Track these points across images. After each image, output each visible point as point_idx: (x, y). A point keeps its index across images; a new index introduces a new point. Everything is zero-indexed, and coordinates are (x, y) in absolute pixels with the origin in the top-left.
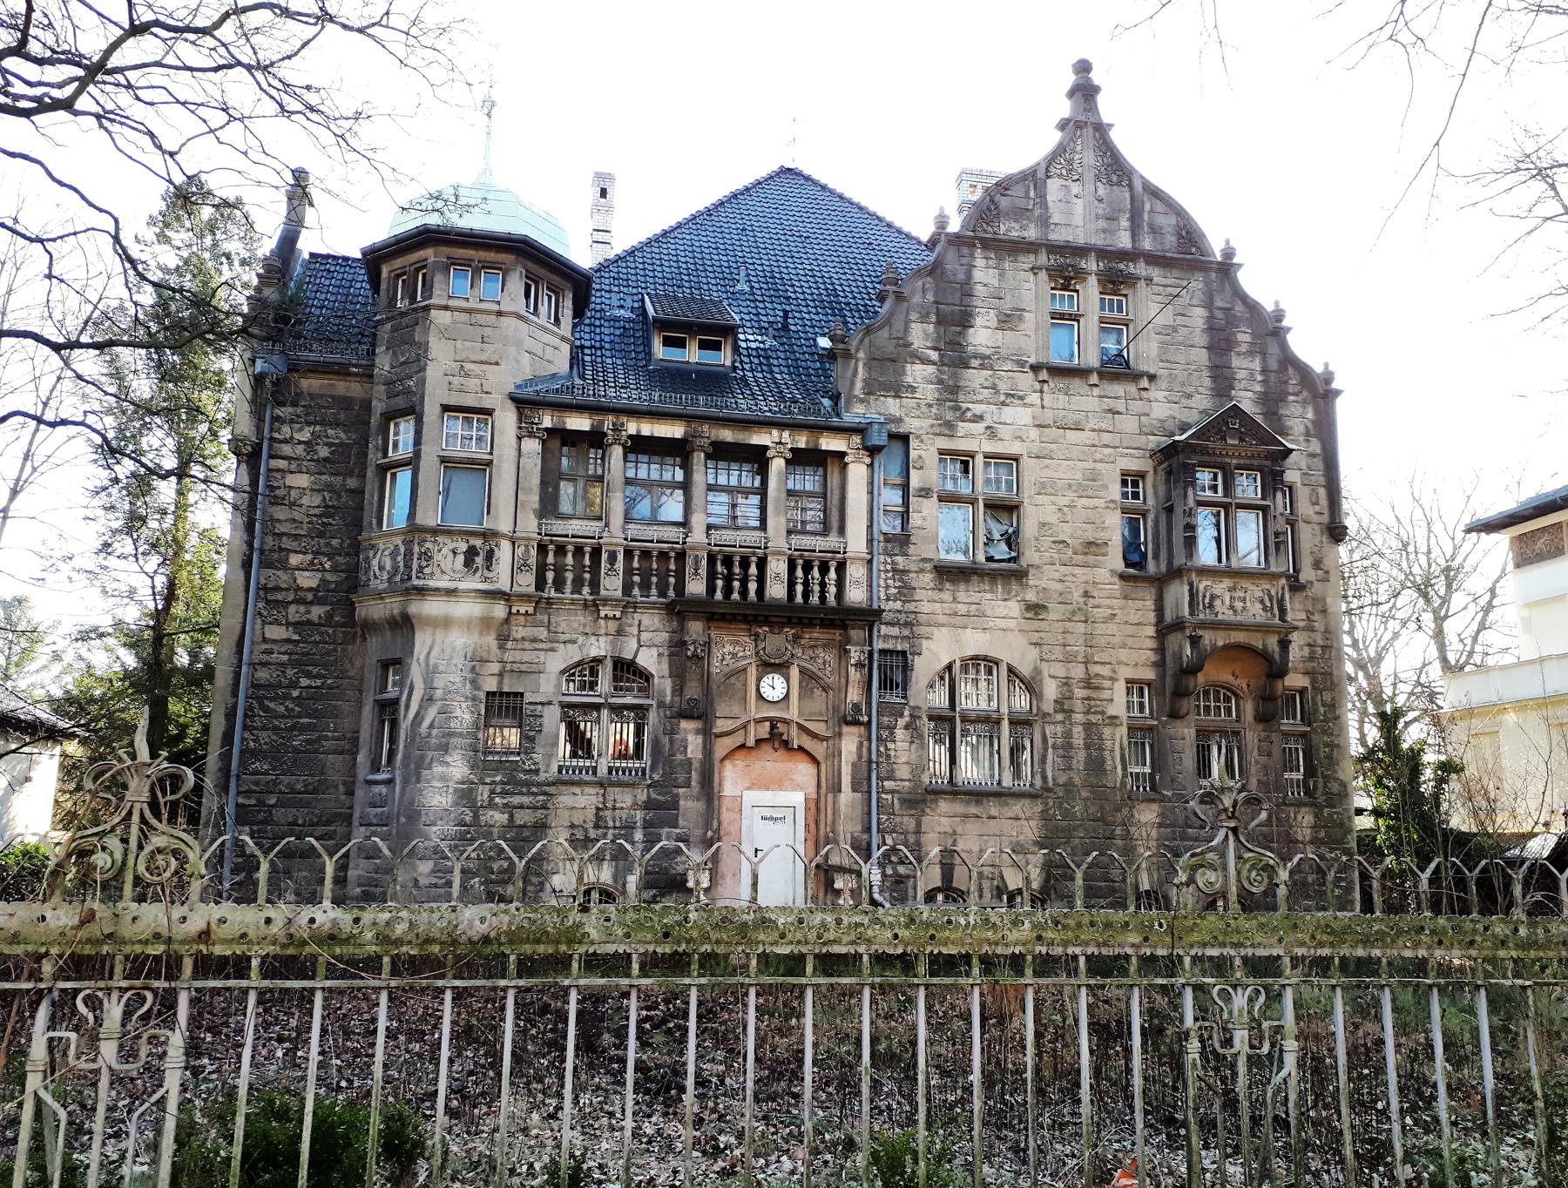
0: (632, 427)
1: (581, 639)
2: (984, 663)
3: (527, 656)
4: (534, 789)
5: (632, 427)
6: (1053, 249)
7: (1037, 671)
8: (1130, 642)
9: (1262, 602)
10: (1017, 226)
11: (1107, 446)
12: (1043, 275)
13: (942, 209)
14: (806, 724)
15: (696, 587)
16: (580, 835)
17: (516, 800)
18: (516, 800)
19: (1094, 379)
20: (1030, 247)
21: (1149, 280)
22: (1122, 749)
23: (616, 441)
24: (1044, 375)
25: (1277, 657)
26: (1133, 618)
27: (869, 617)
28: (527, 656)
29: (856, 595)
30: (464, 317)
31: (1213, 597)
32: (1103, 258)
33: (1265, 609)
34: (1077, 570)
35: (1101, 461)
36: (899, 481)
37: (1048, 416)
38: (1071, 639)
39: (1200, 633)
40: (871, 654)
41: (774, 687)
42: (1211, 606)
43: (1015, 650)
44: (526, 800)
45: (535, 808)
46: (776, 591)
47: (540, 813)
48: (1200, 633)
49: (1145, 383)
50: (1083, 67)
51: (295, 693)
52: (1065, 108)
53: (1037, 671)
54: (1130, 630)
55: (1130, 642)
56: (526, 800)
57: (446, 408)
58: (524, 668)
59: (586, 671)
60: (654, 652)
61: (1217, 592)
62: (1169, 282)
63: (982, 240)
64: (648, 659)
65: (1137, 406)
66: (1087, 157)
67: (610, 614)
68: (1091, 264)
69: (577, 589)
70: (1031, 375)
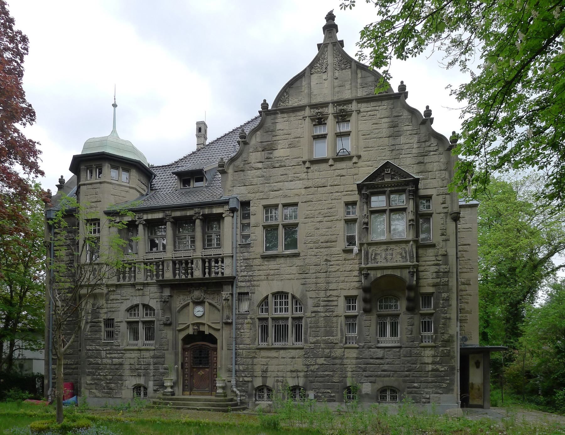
0: (145, 217)
1: (131, 298)
2: (280, 295)
3: (115, 305)
4: (118, 352)
5: (145, 217)
6: (313, 106)
7: (304, 295)
8: (346, 279)
9: (401, 254)
10: (296, 100)
11: (338, 192)
12: (308, 120)
13: (265, 101)
14: (213, 325)
15: (168, 275)
16: (133, 367)
17: (113, 355)
18: (113, 355)
19: (331, 162)
20: (301, 108)
21: (359, 112)
22: (341, 326)
23: (140, 223)
24: (307, 165)
25: (408, 280)
26: (348, 269)
27: (231, 281)
28: (115, 305)
29: (228, 272)
30: (90, 187)
31: (376, 254)
32: (313, 108)
33: (402, 257)
34: (322, 250)
35: (335, 199)
36: (385, 217)
37: (310, 183)
38: (319, 280)
39: (369, 272)
40: (232, 294)
41: (199, 310)
42: (375, 258)
43: (293, 287)
44: (116, 355)
45: (119, 358)
46: (198, 274)
47: (120, 360)
48: (369, 272)
49: (355, 160)
50: (330, 17)
51: (65, 323)
52: (320, 38)
53: (304, 295)
54: (347, 274)
55: (346, 279)
56: (116, 355)
57: (88, 220)
58: (113, 310)
59: (133, 309)
60: (155, 300)
61: (378, 252)
62: (369, 109)
63: (279, 110)
64: (153, 304)
65: (354, 171)
66: (330, 59)
67: (139, 288)
68: (330, 110)
69: (130, 280)
70: (303, 166)
